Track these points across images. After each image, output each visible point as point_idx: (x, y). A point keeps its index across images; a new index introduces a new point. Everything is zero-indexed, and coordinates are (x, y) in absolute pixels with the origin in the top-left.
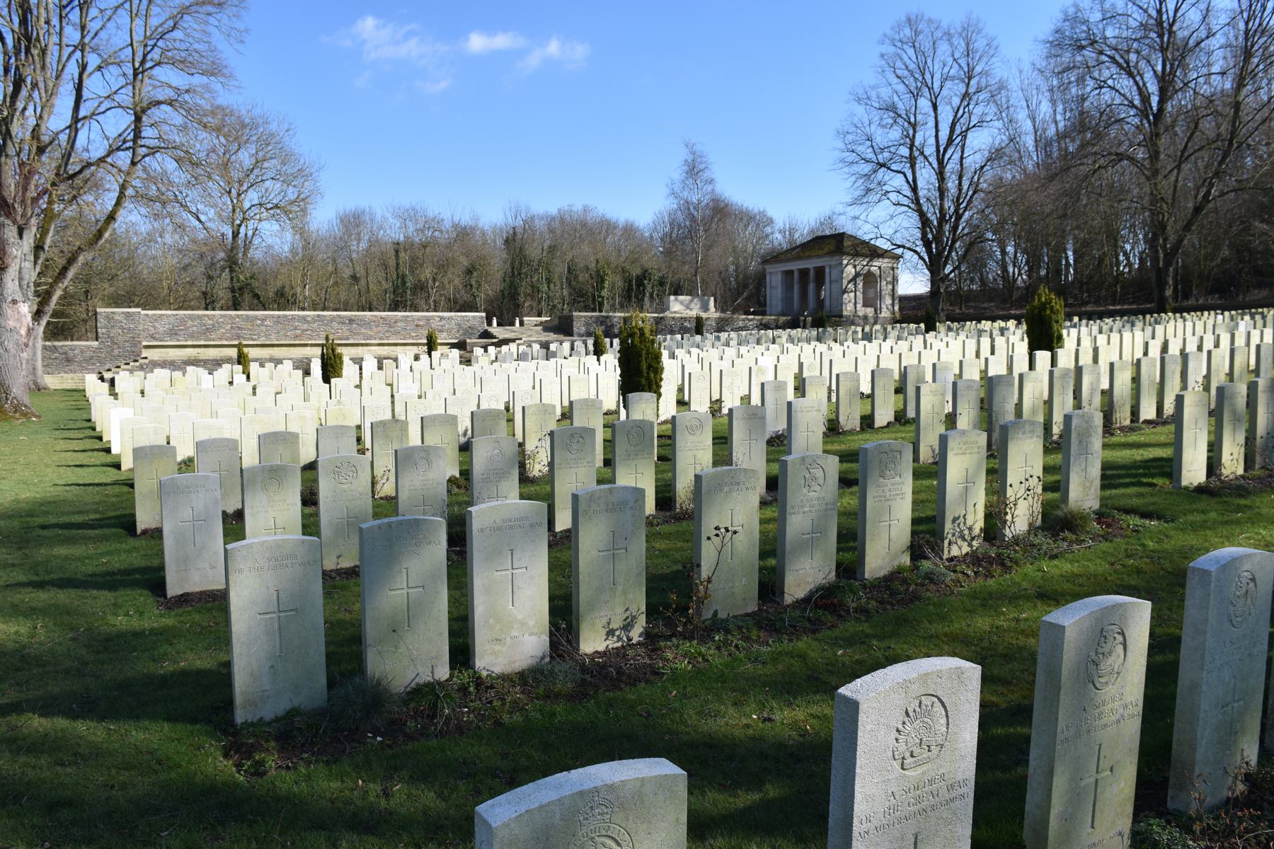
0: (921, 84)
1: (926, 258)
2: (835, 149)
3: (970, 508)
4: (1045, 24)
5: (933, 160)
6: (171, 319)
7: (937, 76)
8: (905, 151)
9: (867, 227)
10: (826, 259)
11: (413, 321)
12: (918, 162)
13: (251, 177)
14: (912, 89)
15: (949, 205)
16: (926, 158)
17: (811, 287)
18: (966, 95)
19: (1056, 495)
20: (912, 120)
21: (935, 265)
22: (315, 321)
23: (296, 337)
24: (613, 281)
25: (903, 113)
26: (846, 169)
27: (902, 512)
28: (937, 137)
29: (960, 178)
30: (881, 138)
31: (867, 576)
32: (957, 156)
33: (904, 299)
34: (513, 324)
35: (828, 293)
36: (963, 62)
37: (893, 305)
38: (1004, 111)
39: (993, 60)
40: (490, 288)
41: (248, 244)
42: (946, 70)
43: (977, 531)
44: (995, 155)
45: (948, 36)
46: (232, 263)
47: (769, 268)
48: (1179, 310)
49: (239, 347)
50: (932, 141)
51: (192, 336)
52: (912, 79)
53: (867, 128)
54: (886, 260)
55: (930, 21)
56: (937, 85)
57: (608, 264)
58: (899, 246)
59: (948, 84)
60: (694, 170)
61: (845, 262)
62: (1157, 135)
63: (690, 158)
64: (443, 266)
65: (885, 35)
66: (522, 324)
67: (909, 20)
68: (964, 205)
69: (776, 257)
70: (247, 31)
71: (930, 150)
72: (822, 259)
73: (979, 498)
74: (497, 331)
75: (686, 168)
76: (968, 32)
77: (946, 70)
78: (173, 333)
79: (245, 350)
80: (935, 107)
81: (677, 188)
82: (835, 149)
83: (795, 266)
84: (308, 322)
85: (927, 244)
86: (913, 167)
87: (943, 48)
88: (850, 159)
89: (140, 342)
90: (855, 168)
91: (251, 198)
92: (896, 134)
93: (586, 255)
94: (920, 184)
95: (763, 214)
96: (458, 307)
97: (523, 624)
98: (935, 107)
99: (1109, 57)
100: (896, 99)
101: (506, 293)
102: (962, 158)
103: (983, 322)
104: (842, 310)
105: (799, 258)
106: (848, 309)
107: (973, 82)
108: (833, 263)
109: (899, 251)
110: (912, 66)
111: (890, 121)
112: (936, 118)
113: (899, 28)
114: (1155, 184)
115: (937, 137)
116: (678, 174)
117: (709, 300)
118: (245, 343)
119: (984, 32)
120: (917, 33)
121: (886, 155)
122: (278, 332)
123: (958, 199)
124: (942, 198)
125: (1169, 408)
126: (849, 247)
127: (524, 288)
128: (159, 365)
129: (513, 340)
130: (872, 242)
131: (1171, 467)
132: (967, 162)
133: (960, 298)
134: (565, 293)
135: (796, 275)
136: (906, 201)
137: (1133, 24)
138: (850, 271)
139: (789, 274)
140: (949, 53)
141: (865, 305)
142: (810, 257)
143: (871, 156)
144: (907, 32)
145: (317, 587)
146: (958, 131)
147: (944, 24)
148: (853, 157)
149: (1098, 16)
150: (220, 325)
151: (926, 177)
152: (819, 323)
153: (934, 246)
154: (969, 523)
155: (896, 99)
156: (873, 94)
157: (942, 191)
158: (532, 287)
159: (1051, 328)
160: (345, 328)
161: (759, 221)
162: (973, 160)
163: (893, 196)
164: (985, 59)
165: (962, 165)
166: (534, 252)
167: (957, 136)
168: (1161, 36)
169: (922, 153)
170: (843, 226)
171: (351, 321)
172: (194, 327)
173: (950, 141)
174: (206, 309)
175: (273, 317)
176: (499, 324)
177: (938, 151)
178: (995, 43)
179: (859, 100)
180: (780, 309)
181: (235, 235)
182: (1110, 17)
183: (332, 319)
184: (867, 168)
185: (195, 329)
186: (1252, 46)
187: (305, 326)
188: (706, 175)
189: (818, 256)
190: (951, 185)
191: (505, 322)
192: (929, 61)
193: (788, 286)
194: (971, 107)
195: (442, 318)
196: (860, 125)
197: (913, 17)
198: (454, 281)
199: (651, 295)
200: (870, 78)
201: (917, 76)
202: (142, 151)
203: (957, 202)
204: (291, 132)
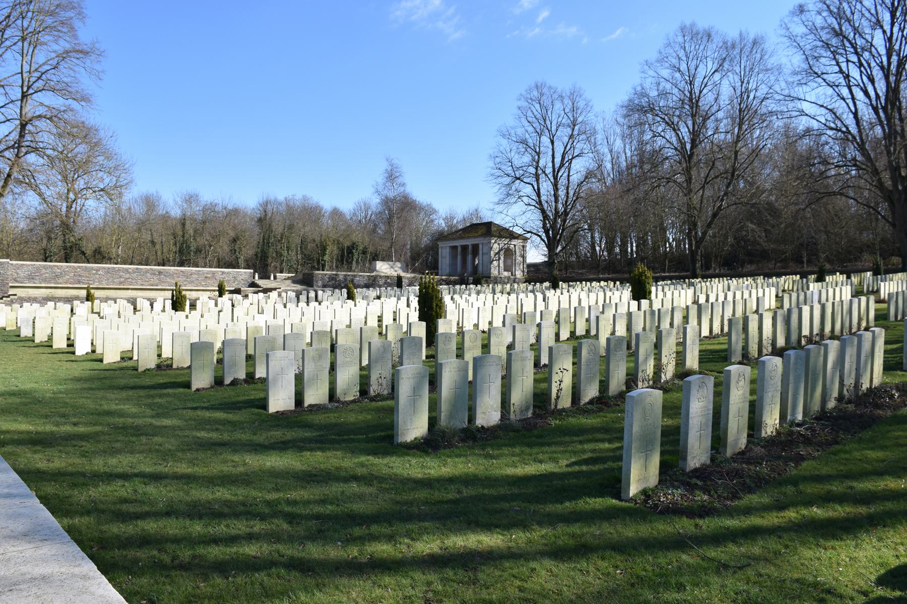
0: (543, 126)
1: (546, 240)
2: (488, 167)
3: (648, 367)
4: (623, 95)
5: (550, 176)
7: (554, 123)
8: (532, 170)
9: (508, 219)
10: (481, 239)
12: (541, 177)
13: (83, 166)
14: (538, 130)
15: (560, 207)
16: (546, 175)
17: (470, 257)
18: (571, 136)
20: (538, 150)
21: (551, 245)
23: (121, 283)
24: (332, 250)
25: (531, 145)
26: (494, 181)
28: (553, 162)
29: (568, 188)
30: (517, 162)
31: (610, 394)
32: (566, 174)
33: (530, 266)
34: (269, 278)
35: (481, 262)
36: (570, 115)
38: (595, 150)
39: (590, 114)
40: (248, 251)
41: (77, 214)
42: (560, 119)
43: (651, 377)
44: (589, 175)
45: (561, 97)
46: (66, 227)
47: (441, 244)
48: (705, 277)
49: (88, 289)
50: (550, 165)
51: (45, 280)
52: (538, 124)
53: (509, 154)
54: (520, 241)
55: (550, 88)
56: (554, 128)
57: (328, 238)
58: (529, 232)
59: (561, 129)
62: (690, 168)
63: (389, 168)
64: (216, 237)
65: (521, 95)
66: (275, 278)
67: (537, 87)
68: (569, 207)
69: (442, 236)
70: (103, 72)
71: (549, 170)
72: (477, 239)
73: (651, 363)
74: (264, 283)
75: (386, 175)
76: (574, 96)
77: (560, 119)
78: (31, 278)
79: (92, 291)
80: (552, 142)
81: (380, 188)
82: (488, 167)
83: (459, 243)
84: (129, 273)
85: (547, 232)
86: (538, 180)
87: (558, 105)
88: (498, 174)
89: (8, 284)
90: (500, 180)
91: (80, 184)
92: (527, 159)
93: (307, 230)
94: (542, 191)
95: (429, 205)
96: (160, 260)
97: (492, 406)
98: (552, 142)
99: (661, 118)
100: (527, 136)
101: (259, 255)
102: (569, 176)
103: (594, 282)
104: (490, 273)
105: (461, 238)
106: (494, 272)
107: (577, 128)
108: (485, 242)
109: (528, 235)
110: (539, 116)
111: (523, 150)
112: (553, 150)
113: (530, 90)
114: (690, 199)
115: (553, 162)
116: (381, 179)
118: (91, 286)
119: (584, 96)
120: (542, 94)
121: (521, 172)
122: (108, 279)
123: (566, 202)
124: (556, 201)
125: (726, 329)
126: (495, 231)
127: (271, 252)
128: (25, 300)
129: (275, 289)
130: (511, 229)
132: (571, 178)
133: (567, 266)
134: (299, 257)
135: (459, 249)
136: (534, 203)
137: (675, 98)
138: (496, 247)
139: (454, 248)
140: (562, 108)
141: (505, 270)
142: (469, 237)
143: (509, 170)
144: (535, 93)
146: (566, 159)
147: (559, 90)
148: (499, 173)
149: (656, 93)
150: (66, 273)
151: (546, 187)
152: (477, 282)
153: (551, 232)
154: (648, 373)
155: (527, 136)
156: (513, 132)
157: (556, 197)
158: (277, 252)
159: (645, 287)
160: (155, 278)
161: (429, 211)
162: (575, 178)
163: (526, 199)
164: (584, 114)
165: (568, 180)
166: (278, 229)
167: (566, 162)
168: (692, 108)
169: (544, 172)
171: (160, 273)
173: (562, 165)
174: (46, 261)
175: (104, 268)
176: (260, 278)
177: (554, 171)
178: (590, 104)
179: (504, 136)
180: (448, 271)
181: (69, 207)
182: (663, 94)
183: (147, 271)
184: (508, 180)
185: (47, 275)
186: (743, 119)
187: (128, 276)
188: (400, 180)
189: (475, 237)
190: (562, 193)
191: (265, 276)
192: (549, 112)
193: (454, 257)
194: (574, 144)
195: (223, 273)
196: (504, 152)
197: (539, 84)
198: (223, 248)
199: (357, 260)
200: (511, 122)
201: (541, 122)
202: (24, 150)
203: (565, 205)
204: (113, 138)
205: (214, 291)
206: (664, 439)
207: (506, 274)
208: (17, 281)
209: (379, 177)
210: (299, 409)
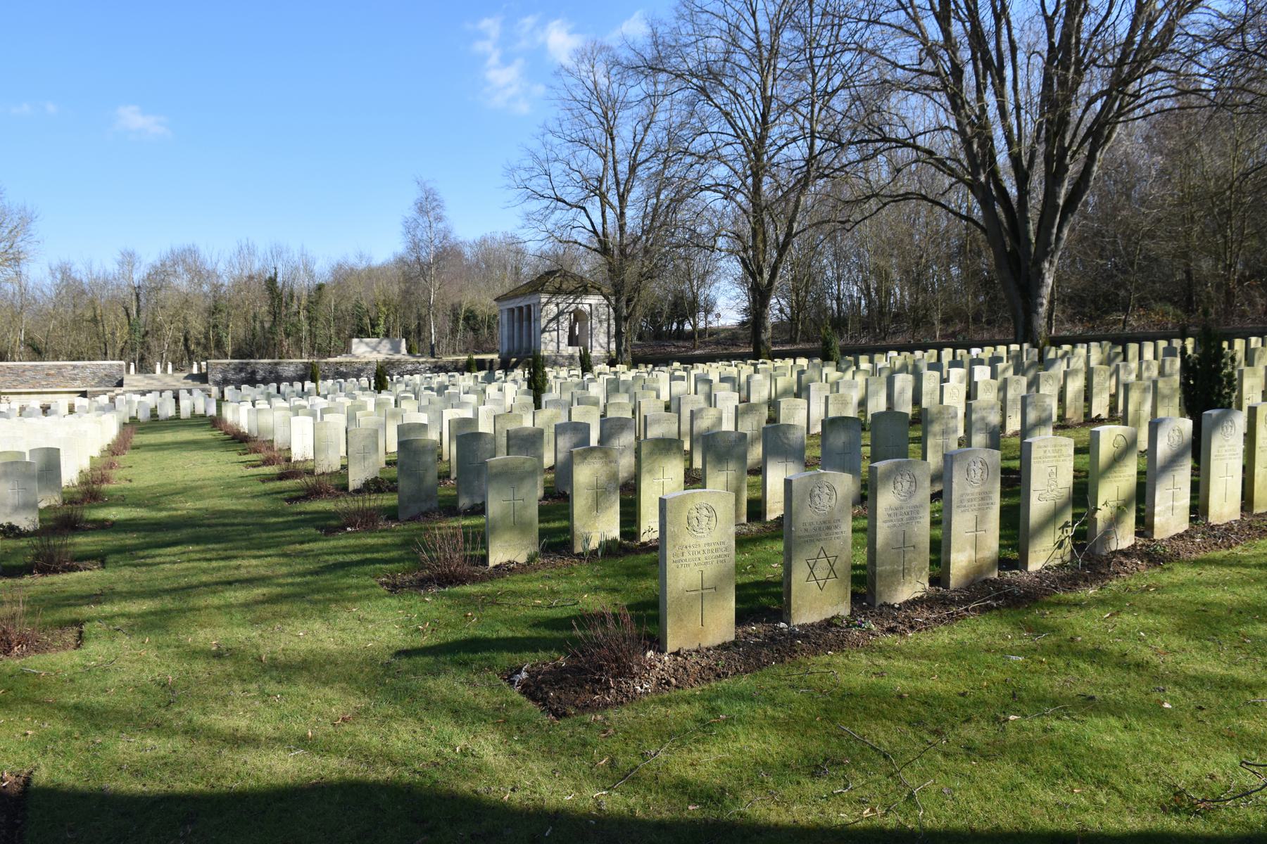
11: (43, 370)
19: (1086, 458)
27: (240, 722)
37: (609, 343)
60: (428, 206)
61: (544, 300)
116: (411, 213)
117: (400, 342)
131: (778, 596)
141: (571, 343)
145: (1256, 363)
195: (75, 367)
206: (1004, 532)
207: (570, 350)
209: (405, 206)
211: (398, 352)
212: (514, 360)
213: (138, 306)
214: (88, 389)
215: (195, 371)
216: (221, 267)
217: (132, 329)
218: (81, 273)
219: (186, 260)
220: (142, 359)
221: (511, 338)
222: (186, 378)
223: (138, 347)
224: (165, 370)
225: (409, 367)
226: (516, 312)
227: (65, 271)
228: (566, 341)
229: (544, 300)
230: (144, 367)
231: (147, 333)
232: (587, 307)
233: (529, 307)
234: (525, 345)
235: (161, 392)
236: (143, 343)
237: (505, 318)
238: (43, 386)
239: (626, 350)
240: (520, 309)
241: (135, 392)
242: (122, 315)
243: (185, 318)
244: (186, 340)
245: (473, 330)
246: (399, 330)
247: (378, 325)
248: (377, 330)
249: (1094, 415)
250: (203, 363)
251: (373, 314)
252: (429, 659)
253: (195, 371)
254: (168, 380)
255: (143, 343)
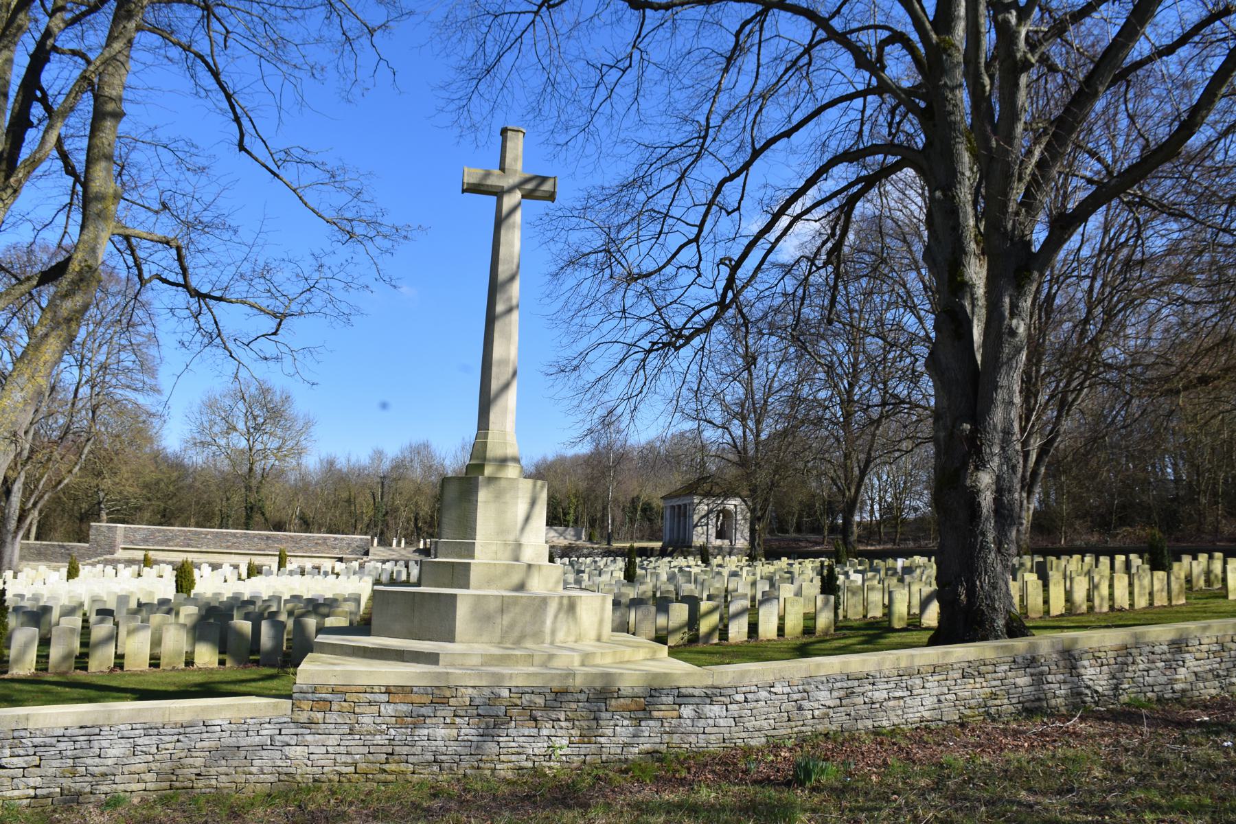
6: (146, 532)
22: (242, 537)
23: (228, 547)
51: (157, 543)
141: (717, 537)
160: (263, 543)
170: (379, 454)
171: (268, 538)
172: (159, 537)
175: (213, 532)
183: (255, 536)
195: (336, 539)
205: (275, 555)
207: (719, 542)
208: (133, 544)
210: (752, 642)
211: (579, 538)
212: (670, 549)
213: (382, 492)
214: (344, 556)
215: (421, 546)
216: (447, 463)
217: (376, 508)
218: (342, 464)
219: (421, 450)
220: (382, 533)
221: (672, 530)
222: (415, 551)
223: (380, 523)
224: (399, 543)
225: (585, 551)
226: (676, 510)
227: (331, 463)
228: (714, 535)
229: (696, 501)
230: (385, 542)
231: (387, 513)
232: (732, 507)
233: (685, 505)
234: (681, 536)
235: (396, 561)
236: (384, 521)
237: (668, 513)
238: (313, 552)
239: (759, 544)
240: (679, 506)
241: (378, 561)
242: (369, 497)
243: (417, 503)
244: (416, 519)
245: (650, 520)
246: (585, 519)
247: (569, 514)
248: (568, 518)
249: (621, 563)
250: (428, 540)
251: (565, 504)
252: (222, 21)
253: (421, 546)
254: (403, 552)
255: (384, 521)
